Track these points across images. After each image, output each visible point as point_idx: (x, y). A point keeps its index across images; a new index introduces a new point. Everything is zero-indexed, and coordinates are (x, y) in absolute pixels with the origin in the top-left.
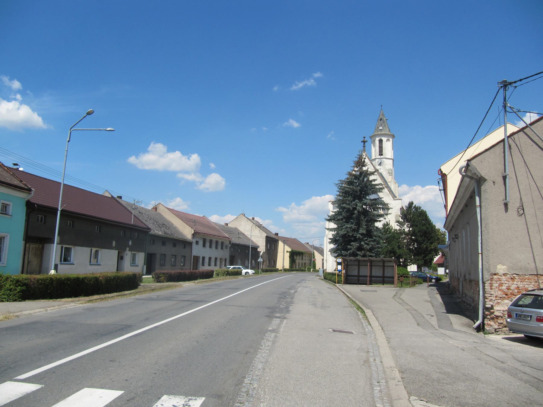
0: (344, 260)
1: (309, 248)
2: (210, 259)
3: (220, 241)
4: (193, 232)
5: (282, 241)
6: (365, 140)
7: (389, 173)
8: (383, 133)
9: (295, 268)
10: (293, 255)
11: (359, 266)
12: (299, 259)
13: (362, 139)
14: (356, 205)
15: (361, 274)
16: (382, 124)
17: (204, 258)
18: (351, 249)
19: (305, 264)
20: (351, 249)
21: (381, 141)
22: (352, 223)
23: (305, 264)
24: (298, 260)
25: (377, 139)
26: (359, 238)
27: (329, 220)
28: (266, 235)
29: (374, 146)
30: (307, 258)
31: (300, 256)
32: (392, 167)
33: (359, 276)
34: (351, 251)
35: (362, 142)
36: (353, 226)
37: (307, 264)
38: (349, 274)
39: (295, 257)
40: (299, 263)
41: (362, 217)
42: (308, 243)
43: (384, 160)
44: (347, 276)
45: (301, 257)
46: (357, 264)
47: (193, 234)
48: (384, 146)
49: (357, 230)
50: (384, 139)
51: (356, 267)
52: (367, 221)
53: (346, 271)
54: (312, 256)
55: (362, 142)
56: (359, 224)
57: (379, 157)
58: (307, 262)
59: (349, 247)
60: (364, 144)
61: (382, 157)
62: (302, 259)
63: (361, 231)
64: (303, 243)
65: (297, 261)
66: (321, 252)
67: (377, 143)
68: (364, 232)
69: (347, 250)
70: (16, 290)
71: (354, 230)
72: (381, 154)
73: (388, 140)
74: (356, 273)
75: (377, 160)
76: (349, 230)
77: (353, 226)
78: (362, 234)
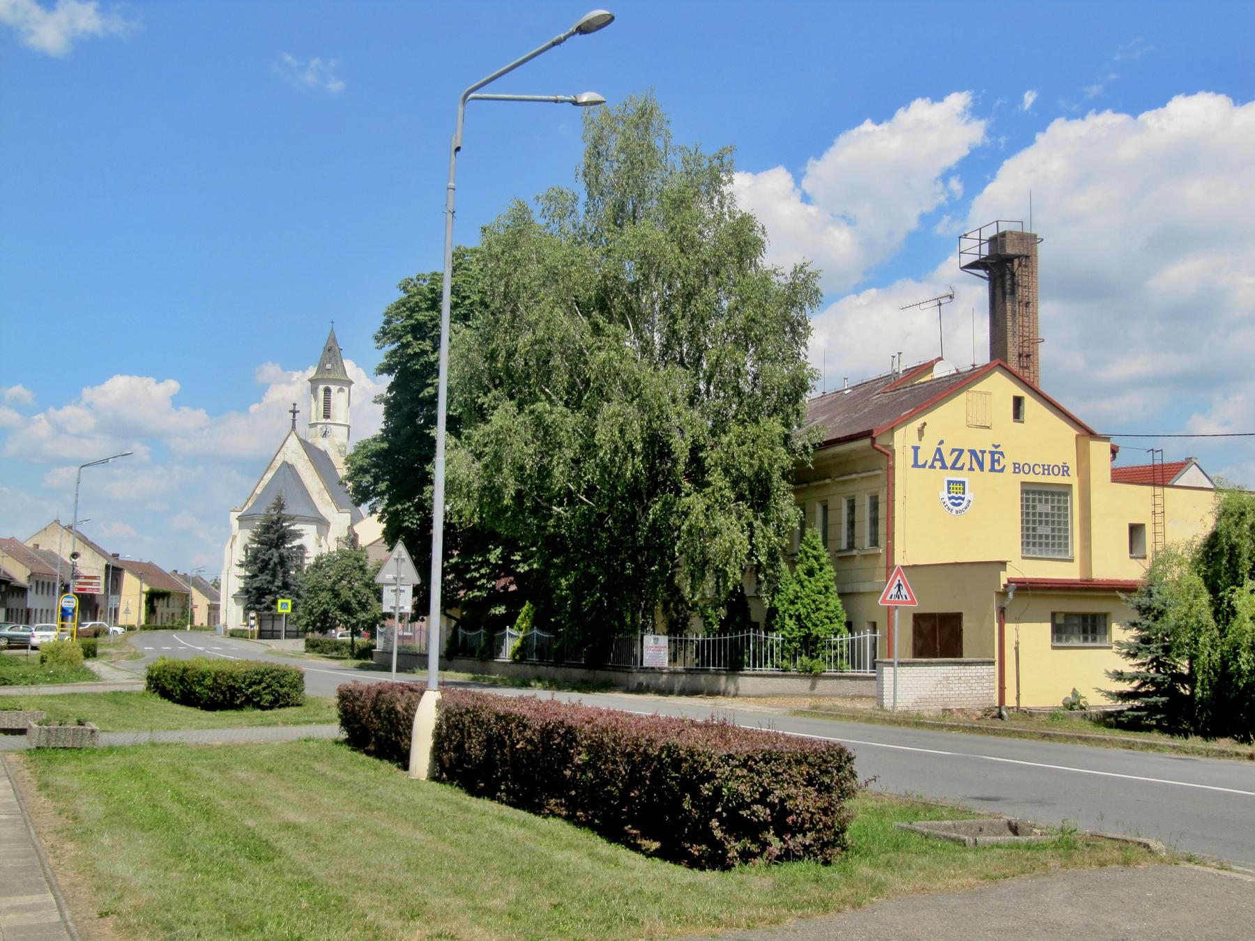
0: (258, 615)
1: (180, 581)
2: (42, 610)
3: (46, 581)
4: (29, 573)
5: (133, 573)
6: (297, 409)
7: (340, 452)
8: (332, 376)
9: (156, 623)
10: (153, 598)
11: (273, 620)
12: (163, 606)
13: (292, 408)
14: (273, 555)
15: (275, 629)
16: (331, 359)
17: (36, 610)
18: (265, 603)
19: (173, 615)
20: (265, 603)
21: (327, 391)
22: (267, 574)
23: (173, 615)
24: (160, 605)
25: (322, 387)
26: (274, 591)
27: (241, 566)
28: (105, 562)
29: (316, 398)
30: (177, 603)
31: (163, 598)
32: (346, 440)
33: (273, 631)
34: (266, 605)
35: (290, 412)
36: (269, 578)
37: (176, 615)
38: (263, 628)
39: (156, 603)
40: (162, 614)
41: (279, 568)
42: (176, 571)
43: (332, 426)
44: (261, 631)
45: (166, 600)
46: (271, 617)
47: (29, 577)
48: (332, 402)
49: (271, 582)
50: (334, 388)
51: (271, 622)
52: (284, 572)
53: (260, 627)
54: (186, 597)
55: (290, 412)
56: (274, 576)
57: (324, 421)
58: (178, 611)
59: (263, 600)
60: (294, 416)
61: (328, 421)
62: (168, 606)
63: (276, 584)
64: (168, 572)
65: (159, 610)
66: (212, 590)
67: (321, 394)
68: (280, 584)
69: (260, 603)
70: (1227, 544)
71: (269, 582)
72: (327, 416)
73: (341, 390)
74: (269, 628)
75: (319, 426)
76: (264, 582)
77: (269, 578)
78: (278, 587)
